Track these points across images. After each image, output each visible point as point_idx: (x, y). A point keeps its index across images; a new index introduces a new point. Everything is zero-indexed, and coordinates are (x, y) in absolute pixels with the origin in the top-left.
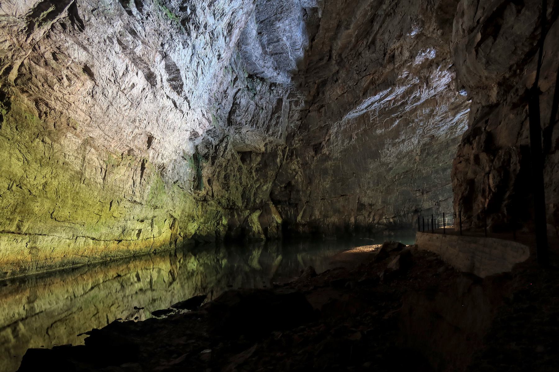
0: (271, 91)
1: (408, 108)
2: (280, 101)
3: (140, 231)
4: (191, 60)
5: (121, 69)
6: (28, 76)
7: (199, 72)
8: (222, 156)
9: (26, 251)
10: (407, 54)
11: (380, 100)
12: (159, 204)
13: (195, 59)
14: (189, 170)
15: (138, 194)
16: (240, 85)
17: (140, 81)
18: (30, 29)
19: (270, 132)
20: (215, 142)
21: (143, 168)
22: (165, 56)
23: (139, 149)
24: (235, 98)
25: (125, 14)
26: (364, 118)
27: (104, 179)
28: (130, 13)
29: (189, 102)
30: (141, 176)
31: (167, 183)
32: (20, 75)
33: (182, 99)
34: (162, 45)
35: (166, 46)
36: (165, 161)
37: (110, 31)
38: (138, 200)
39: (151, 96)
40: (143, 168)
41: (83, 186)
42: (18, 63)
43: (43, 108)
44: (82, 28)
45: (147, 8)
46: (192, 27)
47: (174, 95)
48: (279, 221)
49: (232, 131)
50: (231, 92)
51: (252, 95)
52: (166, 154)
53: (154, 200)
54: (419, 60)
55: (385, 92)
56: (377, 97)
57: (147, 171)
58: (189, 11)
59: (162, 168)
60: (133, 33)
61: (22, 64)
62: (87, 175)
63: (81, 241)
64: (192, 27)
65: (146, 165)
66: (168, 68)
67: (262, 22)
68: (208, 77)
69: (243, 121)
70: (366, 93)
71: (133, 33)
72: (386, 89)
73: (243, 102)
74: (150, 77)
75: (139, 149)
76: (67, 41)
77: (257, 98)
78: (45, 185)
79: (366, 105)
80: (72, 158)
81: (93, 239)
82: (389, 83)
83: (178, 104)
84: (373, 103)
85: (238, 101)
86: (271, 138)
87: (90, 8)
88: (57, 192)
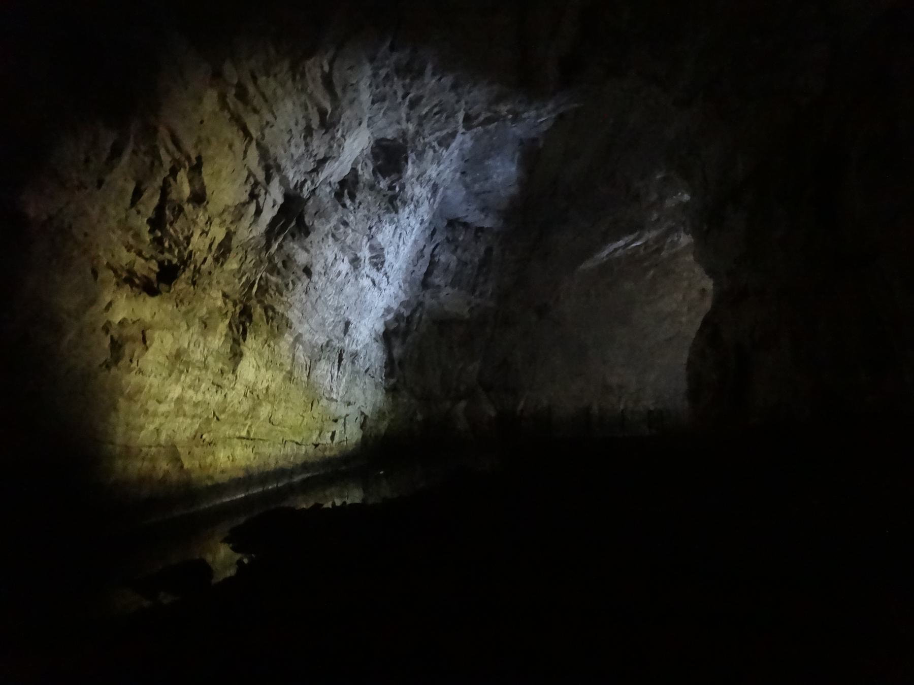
0: (477, 238)
1: (664, 254)
2: (489, 250)
3: (334, 433)
4: (394, 234)
5: (331, 259)
6: (265, 287)
7: (401, 243)
8: (416, 330)
9: (252, 456)
10: (654, 197)
11: (627, 245)
12: (352, 400)
13: (399, 231)
14: (380, 354)
15: (335, 390)
16: (439, 238)
17: (344, 266)
18: (268, 246)
19: (477, 293)
20: (406, 313)
21: (340, 360)
22: (371, 238)
23: (337, 338)
24: (432, 256)
25: (340, 207)
26: (605, 268)
27: (308, 376)
28: (344, 206)
29: (388, 278)
30: (339, 369)
31: (358, 372)
32: (260, 286)
33: (381, 275)
34: (370, 228)
35: (374, 229)
36: (359, 348)
37: (328, 227)
38: (334, 396)
39: (353, 280)
40: (340, 360)
41: (293, 386)
42: (258, 277)
43: (270, 313)
44: (307, 233)
45: (359, 197)
46: (399, 203)
47: (374, 273)
48: (493, 413)
49: (428, 296)
50: (428, 251)
51: (453, 247)
52: (361, 338)
53: (347, 395)
54: (670, 203)
55: (632, 237)
56: (621, 243)
57: (343, 362)
58: (397, 189)
59: (355, 355)
60: (346, 224)
61: (261, 277)
62: (295, 375)
63: (289, 445)
64: (399, 203)
65: (344, 356)
66: (372, 248)
67: (466, 161)
68: (410, 243)
69: (442, 283)
70: (607, 238)
71: (346, 224)
72: (631, 233)
73: (443, 258)
74: (355, 262)
75: (337, 338)
76: (293, 246)
77: (459, 251)
78: (267, 388)
79: (606, 252)
80: (286, 358)
81: (297, 443)
82: (636, 227)
83: (377, 282)
84: (616, 250)
85: (436, 259)
86: (479, 301)
87: (314, 212)
88: (274, 395)
